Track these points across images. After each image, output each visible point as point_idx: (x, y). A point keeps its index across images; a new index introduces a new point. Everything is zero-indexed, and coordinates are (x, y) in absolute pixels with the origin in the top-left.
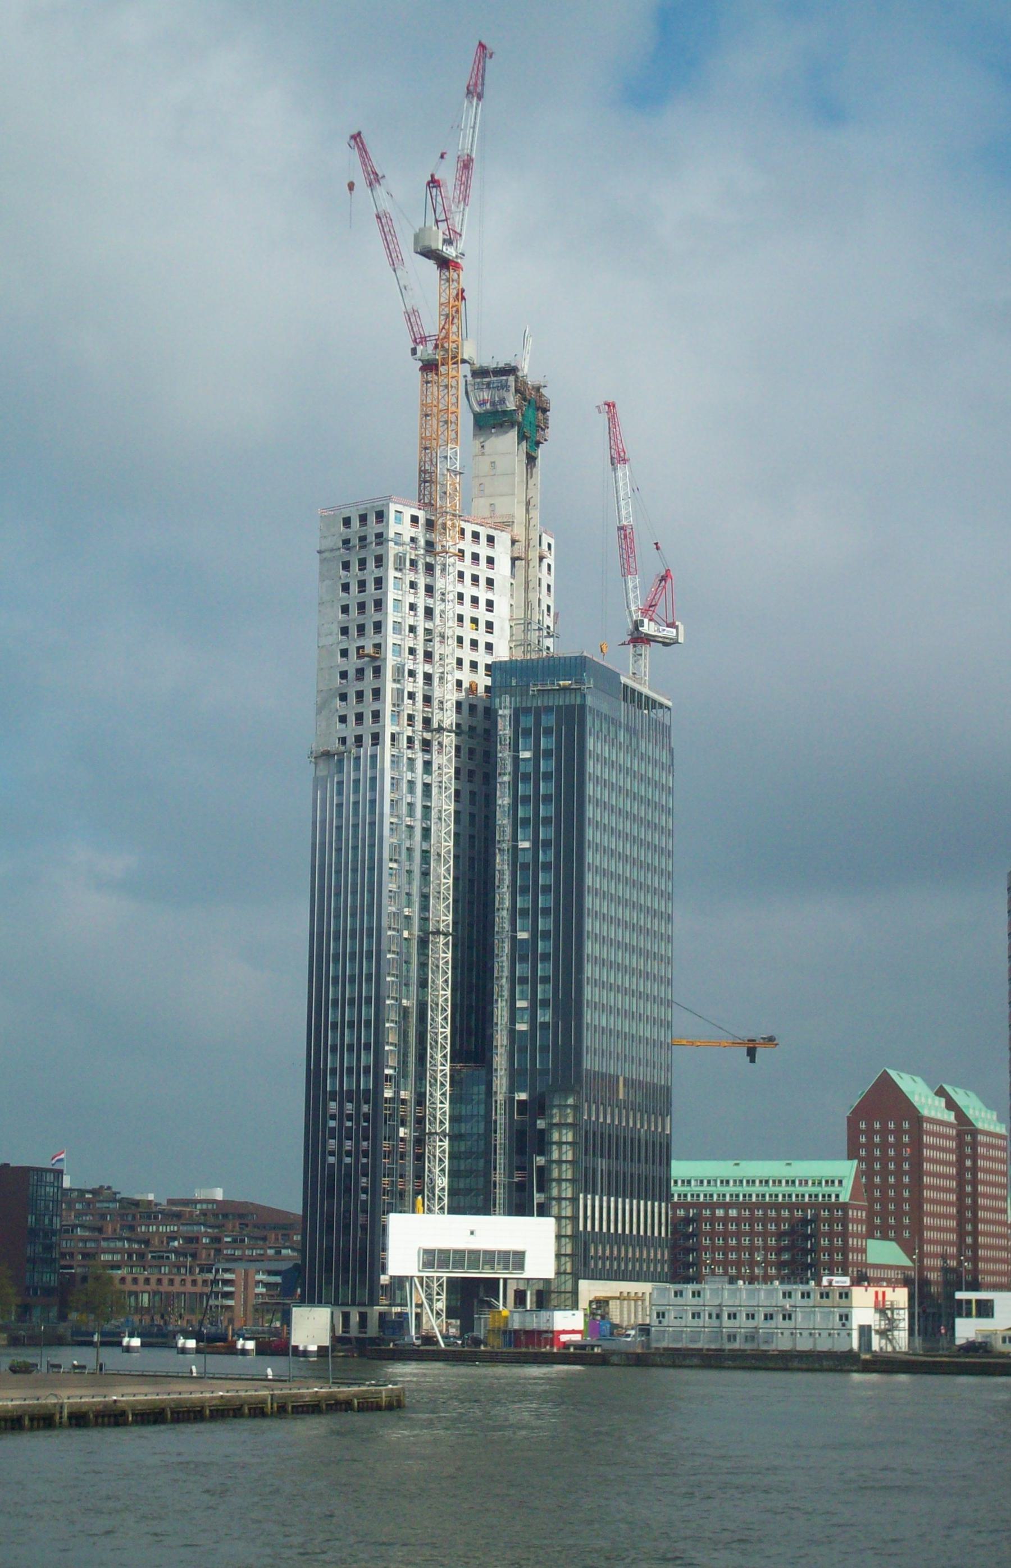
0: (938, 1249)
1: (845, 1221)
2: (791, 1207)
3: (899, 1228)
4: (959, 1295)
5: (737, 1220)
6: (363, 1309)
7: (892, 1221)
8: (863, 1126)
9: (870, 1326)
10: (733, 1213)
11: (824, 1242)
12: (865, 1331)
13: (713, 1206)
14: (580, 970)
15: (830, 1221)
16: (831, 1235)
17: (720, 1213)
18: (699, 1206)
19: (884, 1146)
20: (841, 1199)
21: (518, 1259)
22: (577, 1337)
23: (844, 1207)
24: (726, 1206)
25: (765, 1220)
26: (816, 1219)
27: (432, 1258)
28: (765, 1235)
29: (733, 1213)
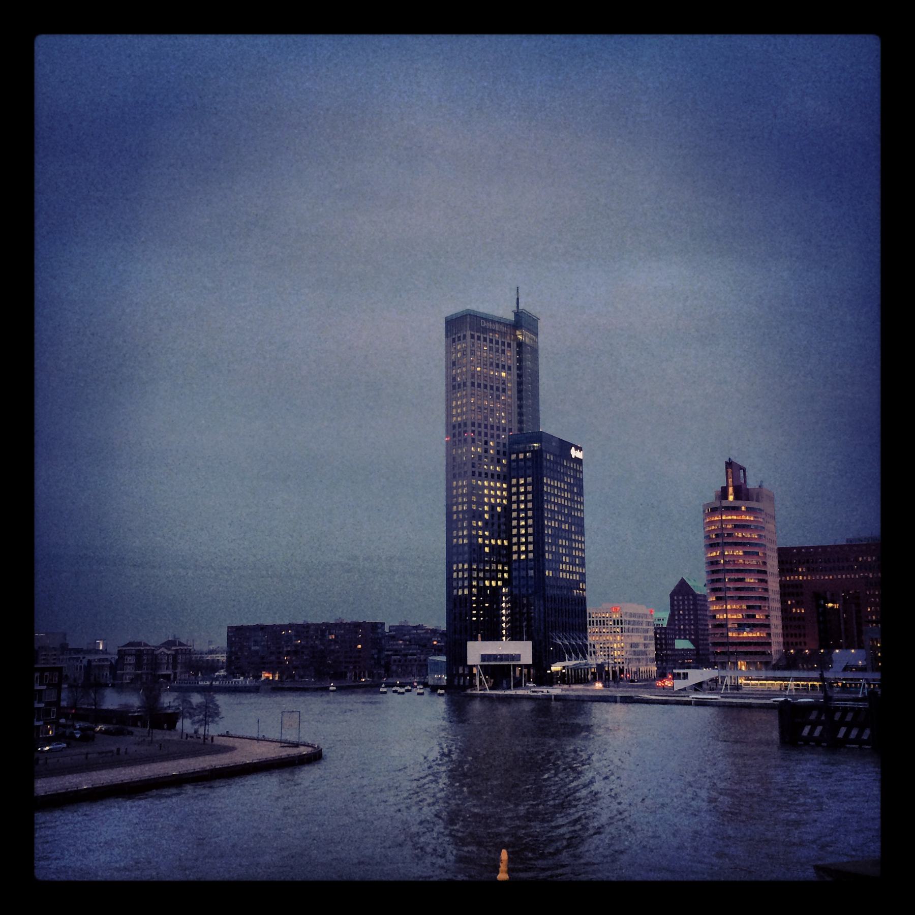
27: (484, 657)
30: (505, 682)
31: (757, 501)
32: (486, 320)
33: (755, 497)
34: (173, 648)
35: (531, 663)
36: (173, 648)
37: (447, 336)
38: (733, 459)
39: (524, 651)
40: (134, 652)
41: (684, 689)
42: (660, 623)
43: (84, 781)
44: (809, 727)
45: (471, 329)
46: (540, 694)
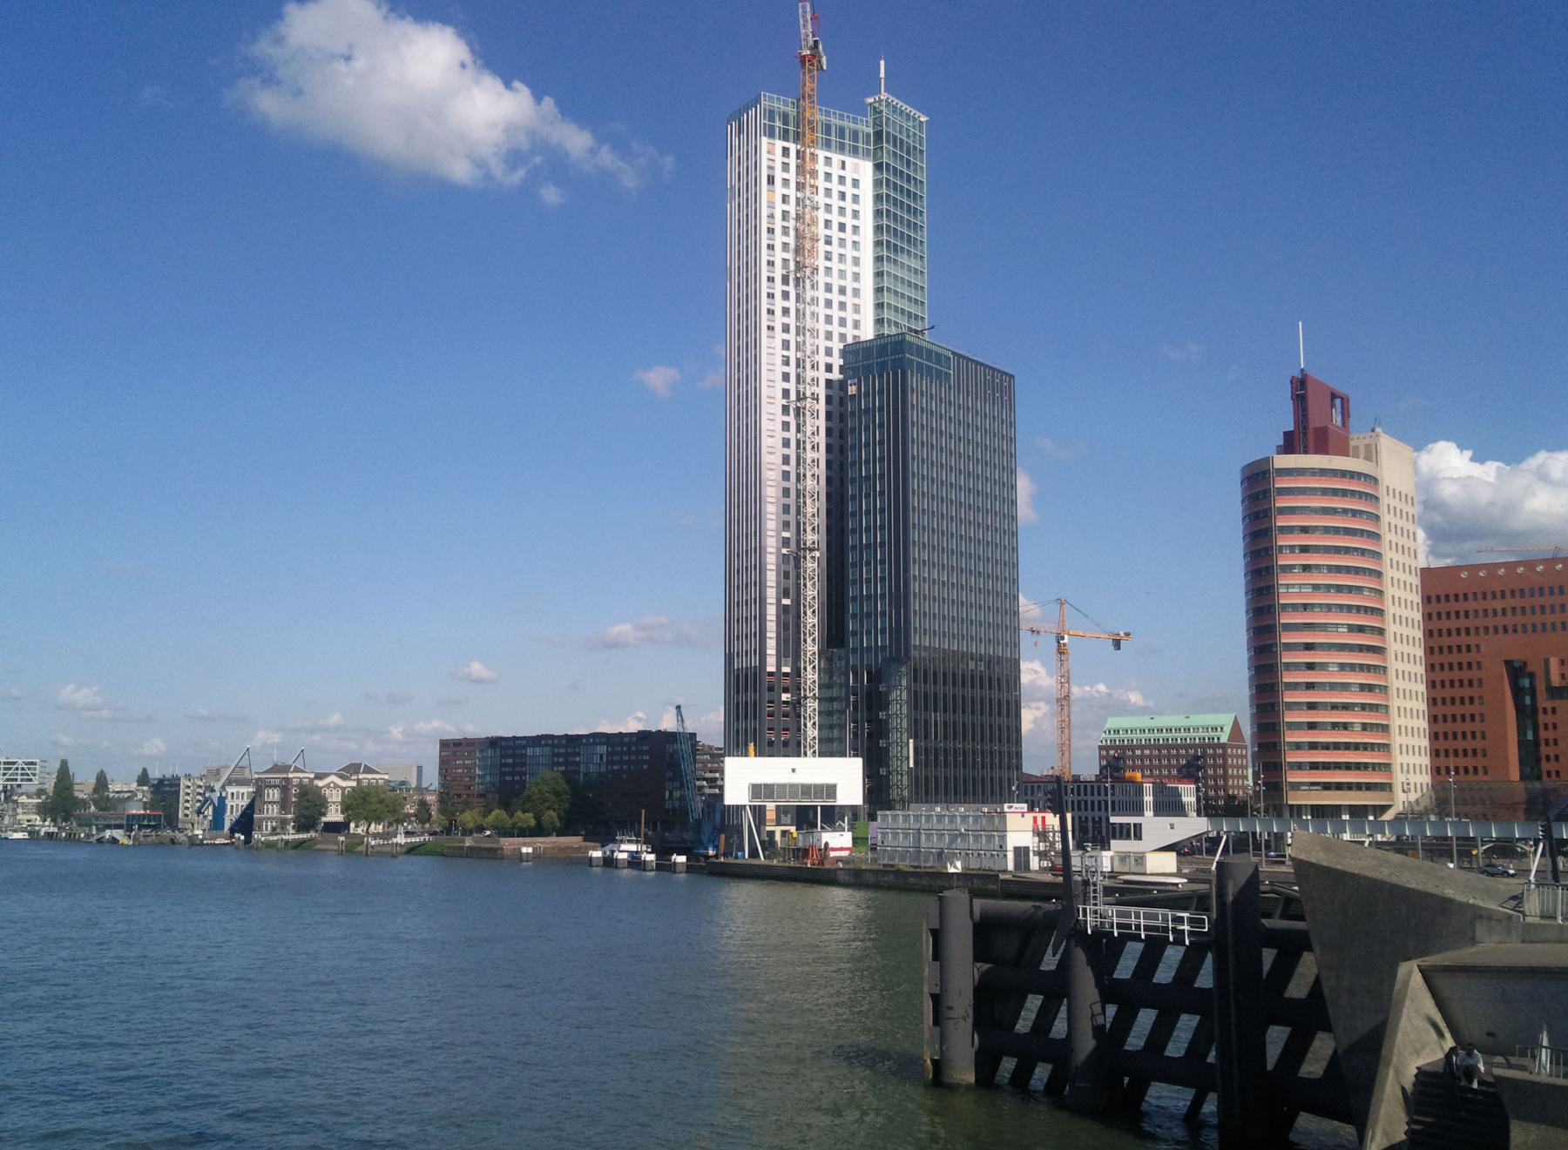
1: (1224, 756)
2: (1187, 747)
5: (1150, 758)
9: (1027, 849)
10: (1147, 752)
11: (1211, 772)
12: (1021, 853)
13: (1133, 748)
14: (906, 570)
15: (1214, 756)
16: (1215, 767)
17: (1138, 752)
18: (1124, 748)
21: (831, 790)
22: (845, 854)
23: (1223, 746)
24: (1142, 747)
25: (1169, 757)
26: (1204, 756)
27: (757, 790)
28: (1169, 767)
29: (1147, 752)
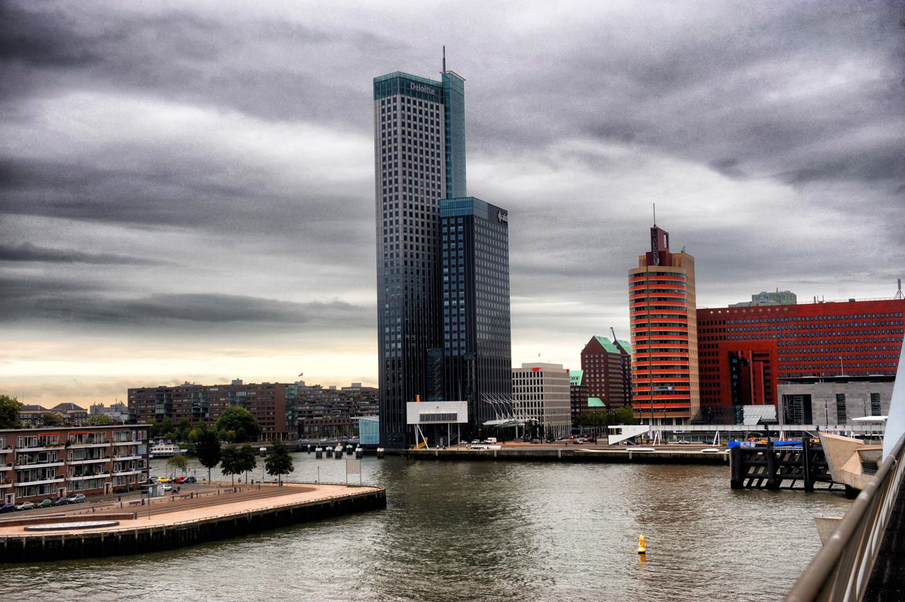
0: (367, 429)
3: (601, 393)
4: (610, 427)
6: (840, 388)
7: (598, 390)
8: (587, 356)
19: (594, 363)
20: (578, 385)
27: (423, 417)
30: (441, 440)
31: (680, 266)
32: (417, 83)
33: (677, 264)
34: (68, 412)
35: (408, 423)
36: (68, 412)
37: (375, 99)
38: (659, 226)
39: (459, 410)
40: (30, 416)
41: (618, 444)
42: (574, 381)
43: (665, 242)
44: (748, 479)
45: (402, 92)
46: (481, 450)
